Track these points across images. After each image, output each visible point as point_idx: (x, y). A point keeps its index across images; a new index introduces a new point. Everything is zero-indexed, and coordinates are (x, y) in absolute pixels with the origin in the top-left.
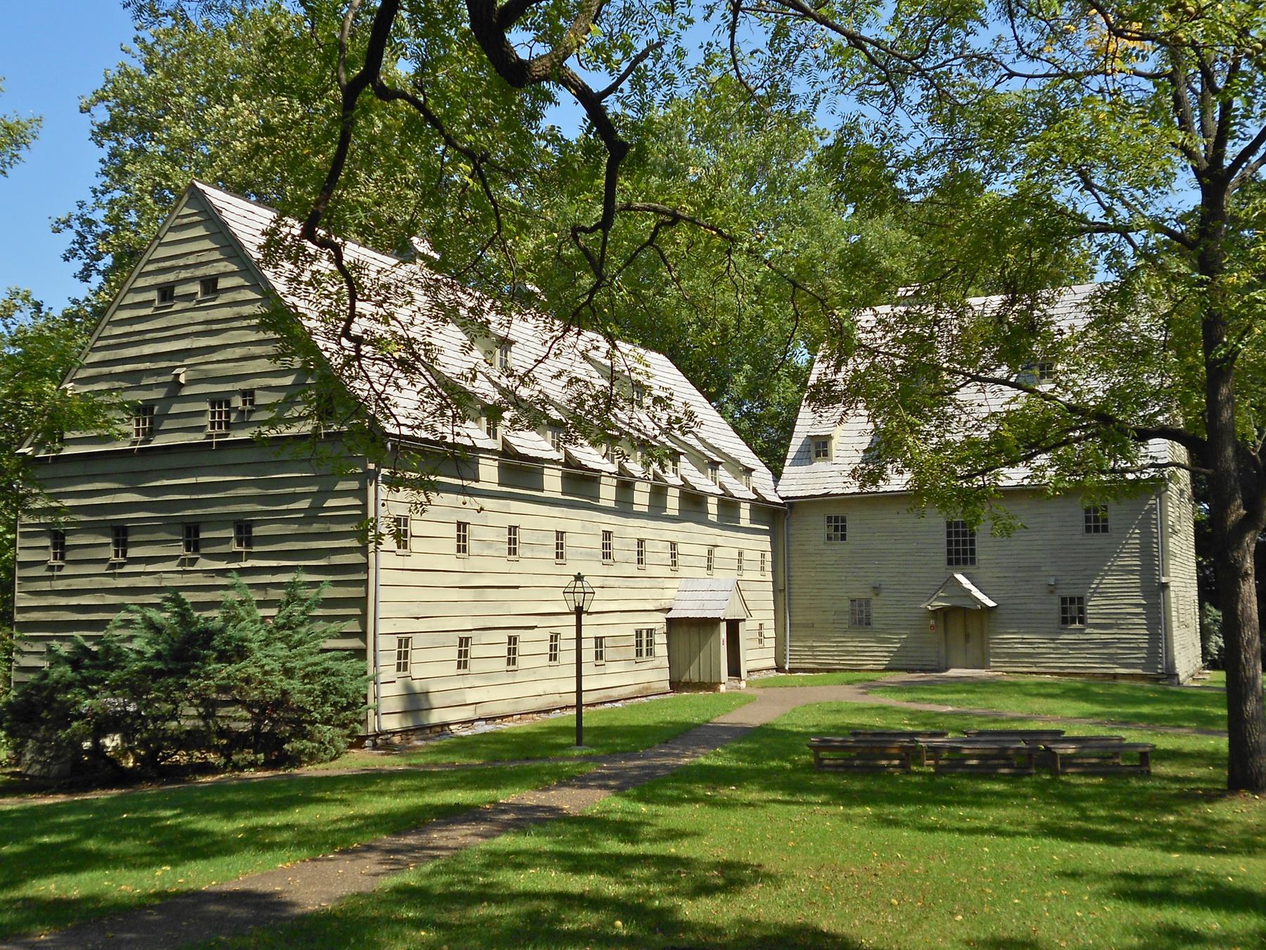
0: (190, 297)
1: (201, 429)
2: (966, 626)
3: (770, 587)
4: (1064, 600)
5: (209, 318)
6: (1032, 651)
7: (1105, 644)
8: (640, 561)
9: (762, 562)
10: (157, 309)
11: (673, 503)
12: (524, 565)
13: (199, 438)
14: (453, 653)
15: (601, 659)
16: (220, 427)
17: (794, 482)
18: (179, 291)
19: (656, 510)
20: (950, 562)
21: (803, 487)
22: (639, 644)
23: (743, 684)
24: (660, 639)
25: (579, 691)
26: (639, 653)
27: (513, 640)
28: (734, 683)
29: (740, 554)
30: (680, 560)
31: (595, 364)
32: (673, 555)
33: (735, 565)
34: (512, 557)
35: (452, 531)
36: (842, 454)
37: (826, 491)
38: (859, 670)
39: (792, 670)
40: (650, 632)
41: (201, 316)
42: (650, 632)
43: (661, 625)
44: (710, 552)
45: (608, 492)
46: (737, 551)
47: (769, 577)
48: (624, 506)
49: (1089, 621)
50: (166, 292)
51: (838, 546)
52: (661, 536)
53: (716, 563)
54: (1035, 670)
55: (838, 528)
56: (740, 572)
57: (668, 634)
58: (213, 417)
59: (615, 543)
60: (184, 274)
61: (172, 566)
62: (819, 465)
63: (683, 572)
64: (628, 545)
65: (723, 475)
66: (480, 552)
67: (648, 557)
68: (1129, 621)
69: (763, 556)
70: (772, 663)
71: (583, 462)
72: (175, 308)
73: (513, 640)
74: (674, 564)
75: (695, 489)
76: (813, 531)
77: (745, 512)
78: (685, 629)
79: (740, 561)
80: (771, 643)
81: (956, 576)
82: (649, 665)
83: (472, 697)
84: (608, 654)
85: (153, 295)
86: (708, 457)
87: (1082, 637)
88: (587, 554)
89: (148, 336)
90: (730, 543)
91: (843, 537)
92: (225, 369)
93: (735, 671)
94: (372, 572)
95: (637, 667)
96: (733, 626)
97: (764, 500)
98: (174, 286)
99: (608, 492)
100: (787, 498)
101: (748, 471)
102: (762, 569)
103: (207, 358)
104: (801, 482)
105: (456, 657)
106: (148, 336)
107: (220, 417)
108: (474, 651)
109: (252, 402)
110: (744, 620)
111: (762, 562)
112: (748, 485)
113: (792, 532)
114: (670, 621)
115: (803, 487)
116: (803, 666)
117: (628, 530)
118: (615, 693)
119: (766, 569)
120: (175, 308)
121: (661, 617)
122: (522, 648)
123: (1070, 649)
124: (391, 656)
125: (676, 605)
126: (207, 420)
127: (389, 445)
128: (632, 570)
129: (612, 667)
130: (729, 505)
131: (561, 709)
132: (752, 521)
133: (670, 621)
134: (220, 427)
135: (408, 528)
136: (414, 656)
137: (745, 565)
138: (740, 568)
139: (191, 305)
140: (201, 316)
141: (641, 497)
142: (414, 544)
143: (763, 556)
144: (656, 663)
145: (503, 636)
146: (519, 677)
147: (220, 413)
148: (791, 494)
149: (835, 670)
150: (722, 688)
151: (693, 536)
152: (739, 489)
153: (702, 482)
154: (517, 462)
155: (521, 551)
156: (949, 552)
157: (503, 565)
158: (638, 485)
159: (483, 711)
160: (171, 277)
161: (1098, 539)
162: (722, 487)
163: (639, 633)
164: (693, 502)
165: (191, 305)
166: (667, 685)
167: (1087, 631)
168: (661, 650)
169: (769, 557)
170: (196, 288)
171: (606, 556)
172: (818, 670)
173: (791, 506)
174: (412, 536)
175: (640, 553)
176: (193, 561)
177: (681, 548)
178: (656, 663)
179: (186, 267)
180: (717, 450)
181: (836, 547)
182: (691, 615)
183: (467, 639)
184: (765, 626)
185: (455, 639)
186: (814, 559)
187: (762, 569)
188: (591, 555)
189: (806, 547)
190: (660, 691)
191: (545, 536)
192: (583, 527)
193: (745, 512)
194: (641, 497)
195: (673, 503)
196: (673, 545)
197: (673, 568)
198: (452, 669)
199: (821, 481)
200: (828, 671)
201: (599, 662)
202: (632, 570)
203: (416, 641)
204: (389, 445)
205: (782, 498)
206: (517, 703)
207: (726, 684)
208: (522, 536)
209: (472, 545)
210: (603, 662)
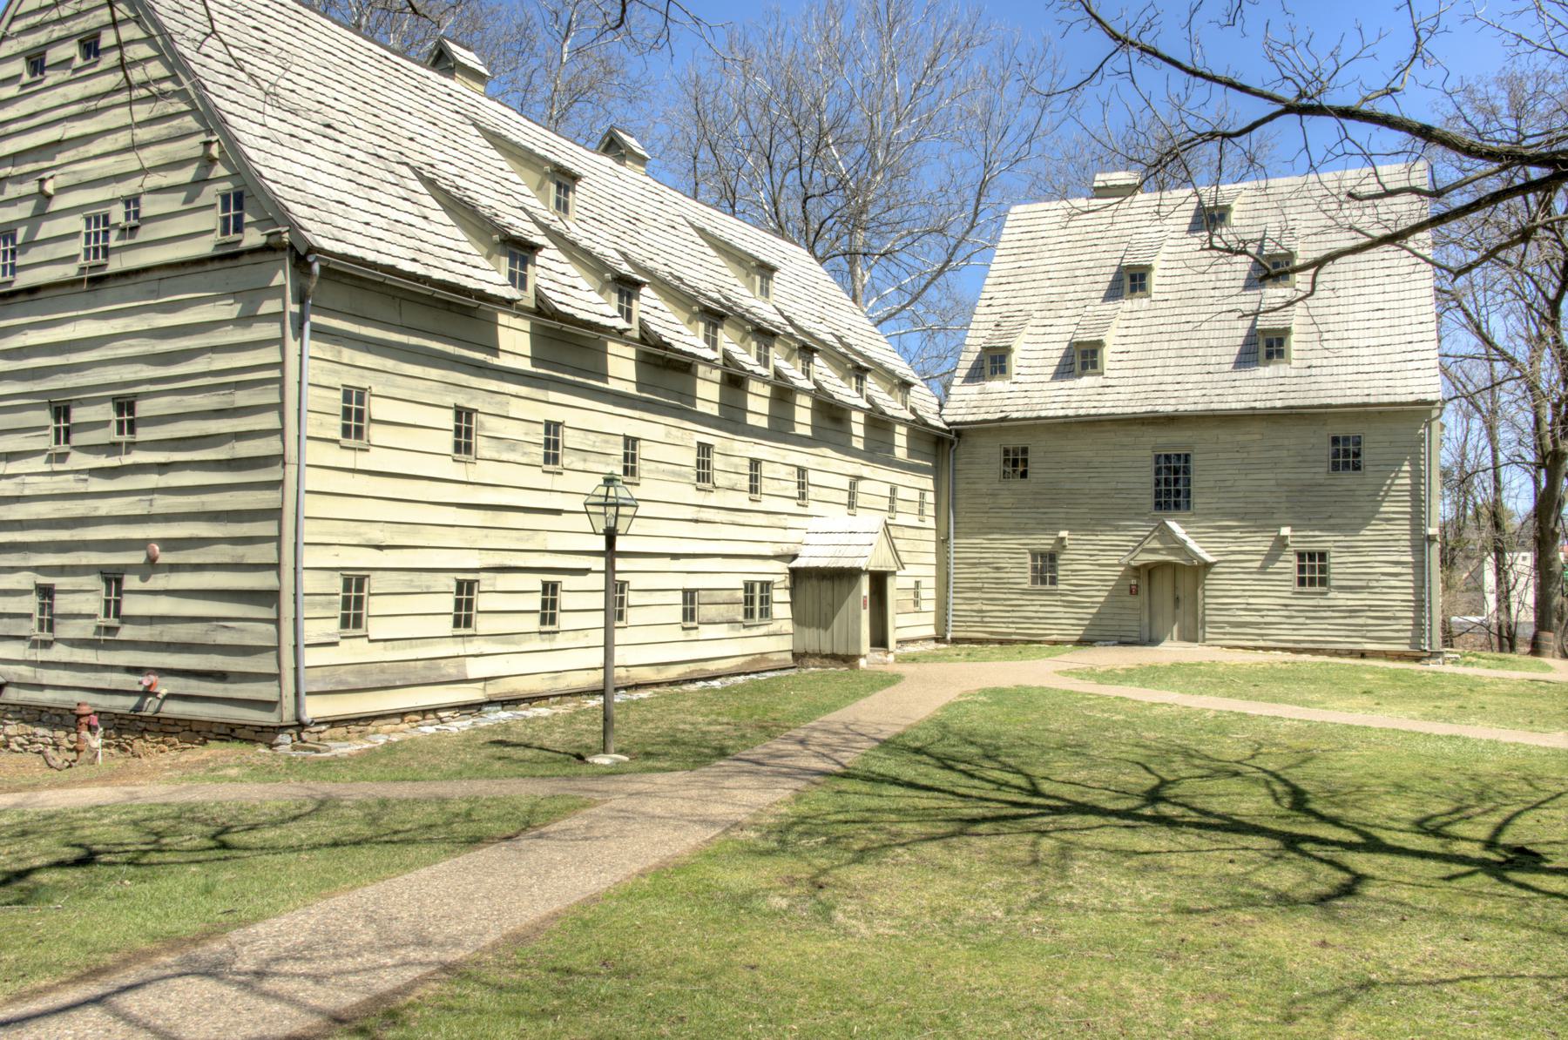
0: (65, 63)
1: (72, 259)
2: (1175, 588)
3: (932, 535)
4: (1301, 556)
5: (87, 93)
6: (1261, 620)
7: (1353, 612)
8: (753, 489)
9: (922, 504)
10: (24, 86)
11: (803, 416)
12: (568, 481)
13: (70, 271)
14: (448, 603)
15: (692, 619)
16: (96, 257)
17: (963, 404)
18: (53, 56)
19: (780, 429)
20: (1158, 505)
21: (975, 410)
22: (749, 601)
23: (891, 658)
24: (781, 595)
25: (607, 665)
26: (749, 613)
27: (550, 589)
28: (879, 655)
29: (893, 491)
30: (812, 492)
31: (708, 238)
32: (801, 485)
33: (885, 504)
34: (551, 467)
35: (448, 419)
36: (1023, 371)
37: (1003, 415)
38: (1040, 642)
39: (955, 641)
40: (766, 586)
41: (76, 91)
42: (766, 586)
43: (782, 577)
44: (853, 485)
45: (708, 392)
46: (888, 487)
47: (930, 522)
48: (732, 418)
49: (1333, 583)
50: (36, 61)
51: (1017, 484)
52: (784, 457)
53: (861, 500)
54: (1261, 643)
55: (1016, 462)
56: (892, 515)
57: (793, 590)
58: (88, 241)
59: (717, 462)
60: (58, 31)
61: (38, 464)
62: (995, 385)
63: (813, 508)
64: (736, 466)
65: (872, 385)
66: (496, 456)
67: (766, 486)
68: (1384, 584)
69: (922, 496)
70: (931, 631)
71: (664, 339)
72: (48, 82)
73: (550, 589)
74: (803, 496)
75: (832, 397)
76: (986, 461)
77: (901, 437)
78: (815, 582)
79: (892, 500)
80: (929, 606)
81: (1169, 523)
82: (763, 630)
83: (475, 669)
84: (704, 612)
85: (19, 66)
86: (852, 361)
87: (1323, 603)
88: (674, 473)
89: (12, 128)
90: (878, 479)
91: (1024, 475)
92: (102, 168)
93: (880, 641)
94: (291, 471)
95: (745, 632)
96: (879, 580)
97: (926, 424)
98: (44, 53)
99: (708, 392)
100: (954, 423)
101: (906, 385)
102: (921, 512)
103: (83, 151)
104: (973, 404)
105: (539, 607)
106: (12, 128)
107: (97, 240)
108: (482, 602)
109: (136, 213)
110: (893, 573)
111: (922, 504)
112: (904, 403)
113: (959, 467)
114: (795, 574)
115: (975, 410)
116: (969, 635)
117: (734, 451)
118: (712, 667)
119: (927, 512)
120: (48, 82)
121: (782, 567)
122: (565, 600)
123: (1307, 618)
124: (331, 603)
125: (802, 551)
126: (78, 247)
127: (316, 267)
128: (742, 500)
129: (706, 631)
130: (879, 423)
131: (626, 688)
132: (912, 451)
133: (795, 574)
134: (96, 257)
135: (365, 407)
136: (374, 606)
137: (899, 505)
138: (892, 509)
139: (67, 75)
140: (76, 91)
141: (758, 404)
142: (376, 434)
143: (922, 496)
144: (774, 627)
145: (535, 582)
146: (560, 640)
147: (97, 234)
148: (958, 419)
149: (1010, 642)
150: (862, 663)
151: (828, 467)
152: (891, 405)
153: (843, 391)
154: (556, 324)
155: (566, 460)
156: (1158, 494)
157: (536, 477)
158: (754, 386)
159: (494, 690)
160: (41, 37)
161: (1347, 479)
162: (869, 399)
163: (749, 587)
164: (831, 415)
165: (67, 75)
166: (789, 656)
167: (1330, 595)
168: (782, 610)
169: (930, 497)
170: (71, 50)
171: (702, 477)
172: (988, 641)
173: (959, 434)
174: (372, 421)
175: (754, 479)
176: (62, 457)
177: (813, 477)
178: (774, 627)
179: (61, 20)
180: (868, 359)
181: (1015, 486)
182: (822, 563)
183: (471, 584)
184: (923, 585)
185: (448, 581)
186: (986, 501)
187: (921, 512)
188: (679, 475)
189: (977, 486)
190: (782, 664)
191: (607, 442)
192: (668, 434)
193: (901, 437)
194: (758, 404)
195: (803, 416)
196: (802, 471)
197: (800, 502)
198: (446, 625)
199: (997, 403)
200: (1001, 642)
201: (689, 624)
202: (742, 500)
203: (376, 583)
204: (316, 267)
205: (948, 424)
206: (556, 678)
207: (869, 659)
208: (569, 438)
209: (482, 446)
210: (695, 624)
